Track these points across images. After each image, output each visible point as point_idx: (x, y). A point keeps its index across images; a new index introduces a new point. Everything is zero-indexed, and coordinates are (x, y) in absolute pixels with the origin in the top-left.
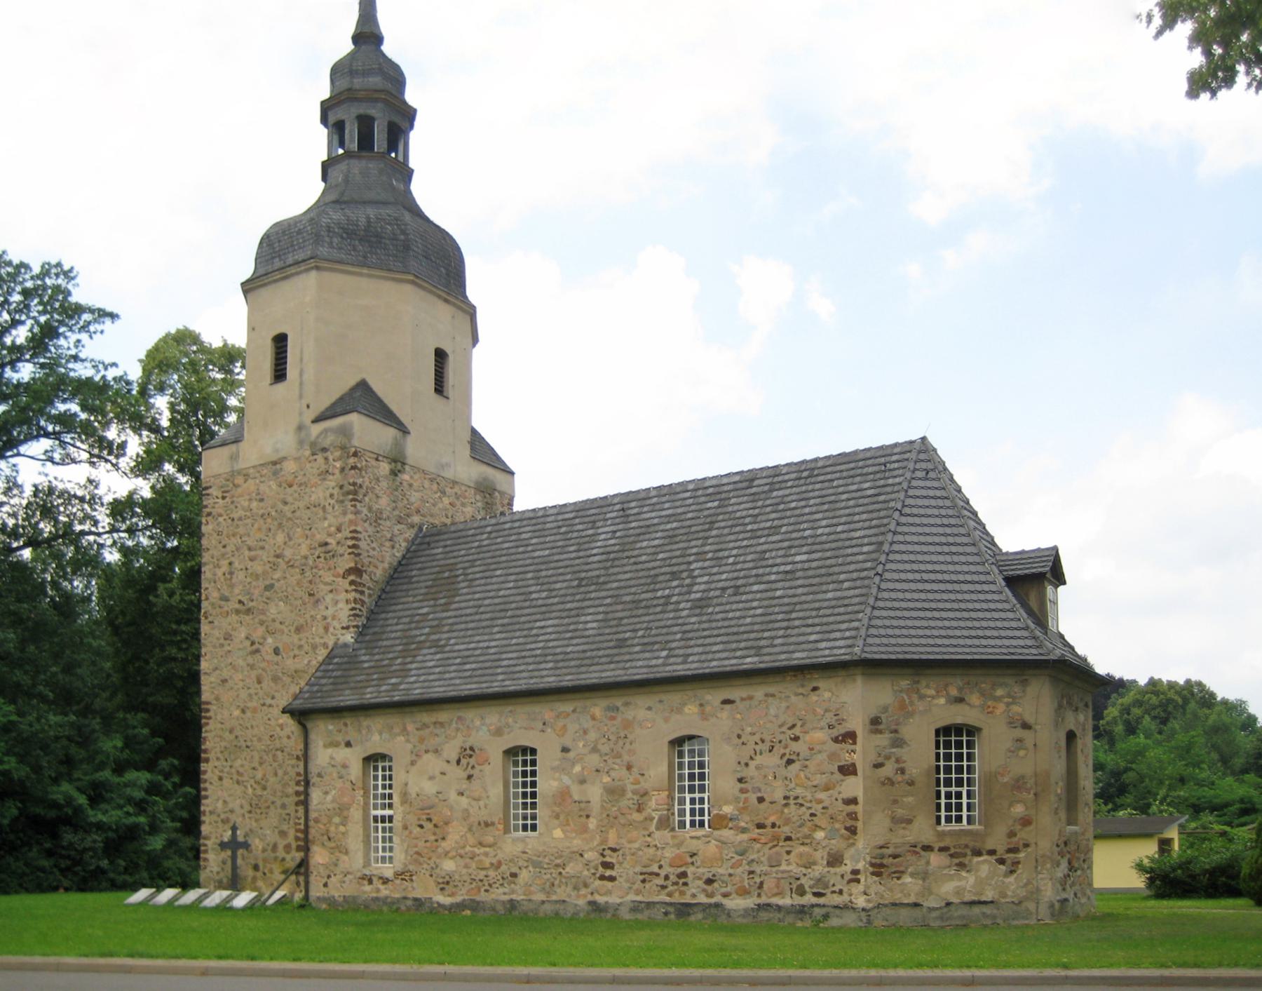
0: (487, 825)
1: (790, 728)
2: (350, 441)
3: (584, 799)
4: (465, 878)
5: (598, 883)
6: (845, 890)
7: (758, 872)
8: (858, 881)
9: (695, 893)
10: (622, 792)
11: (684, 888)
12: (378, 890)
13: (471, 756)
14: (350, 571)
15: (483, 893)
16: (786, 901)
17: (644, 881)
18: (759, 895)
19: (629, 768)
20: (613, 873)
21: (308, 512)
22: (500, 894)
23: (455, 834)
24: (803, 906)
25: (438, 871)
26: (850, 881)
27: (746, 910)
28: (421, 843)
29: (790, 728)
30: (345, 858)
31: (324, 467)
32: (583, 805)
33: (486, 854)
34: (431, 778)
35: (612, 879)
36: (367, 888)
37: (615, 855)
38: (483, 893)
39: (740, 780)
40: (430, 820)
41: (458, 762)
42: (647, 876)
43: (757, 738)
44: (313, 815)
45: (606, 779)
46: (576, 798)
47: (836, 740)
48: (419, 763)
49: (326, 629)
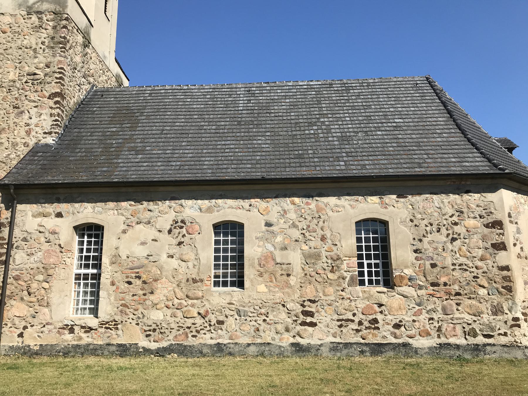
0: (195, 281)
1: (451, 217)
2: (63, 10)
3: (286, 262)
4: (173, 325)
5: (299, 328)
6: (509, 332)
7: (436, 318)
8: (519, 326)
9: (385, 335)
10: (317, 256)
11: (376, 332)
12: (80, 338)
13: (181, 227)
14: (52, 96)
15: (190, 338)
16: (462, 341)
17: (340, 326)
18: (439, 337)
19: (323, 239)
20: (314, 320)
21: (20, 51)
22: (207, 339)
23: (164, 290)
24: (478, 345)
25: (145, 320)
26: (512, 326)
27: (430, 348)
28: (129, 298)
29: (451, 217)
30: (46, 310)
31: (37, 23)
32: (284, 267)
33: (193, 306)
34: (143, 243)
35: (313, 325)
36: (68, 337)
37: (314, 305)
38: (190, 338)
39: (416, 251)
40: (139, 277)
41: (170, 232)
42: (343, 323)
43: (426, 222)
44: (12, 273)
45: (305, 247)
46: (278, 260)
47: (487, 226)
48: (130, 232)
49: (28, 133)
